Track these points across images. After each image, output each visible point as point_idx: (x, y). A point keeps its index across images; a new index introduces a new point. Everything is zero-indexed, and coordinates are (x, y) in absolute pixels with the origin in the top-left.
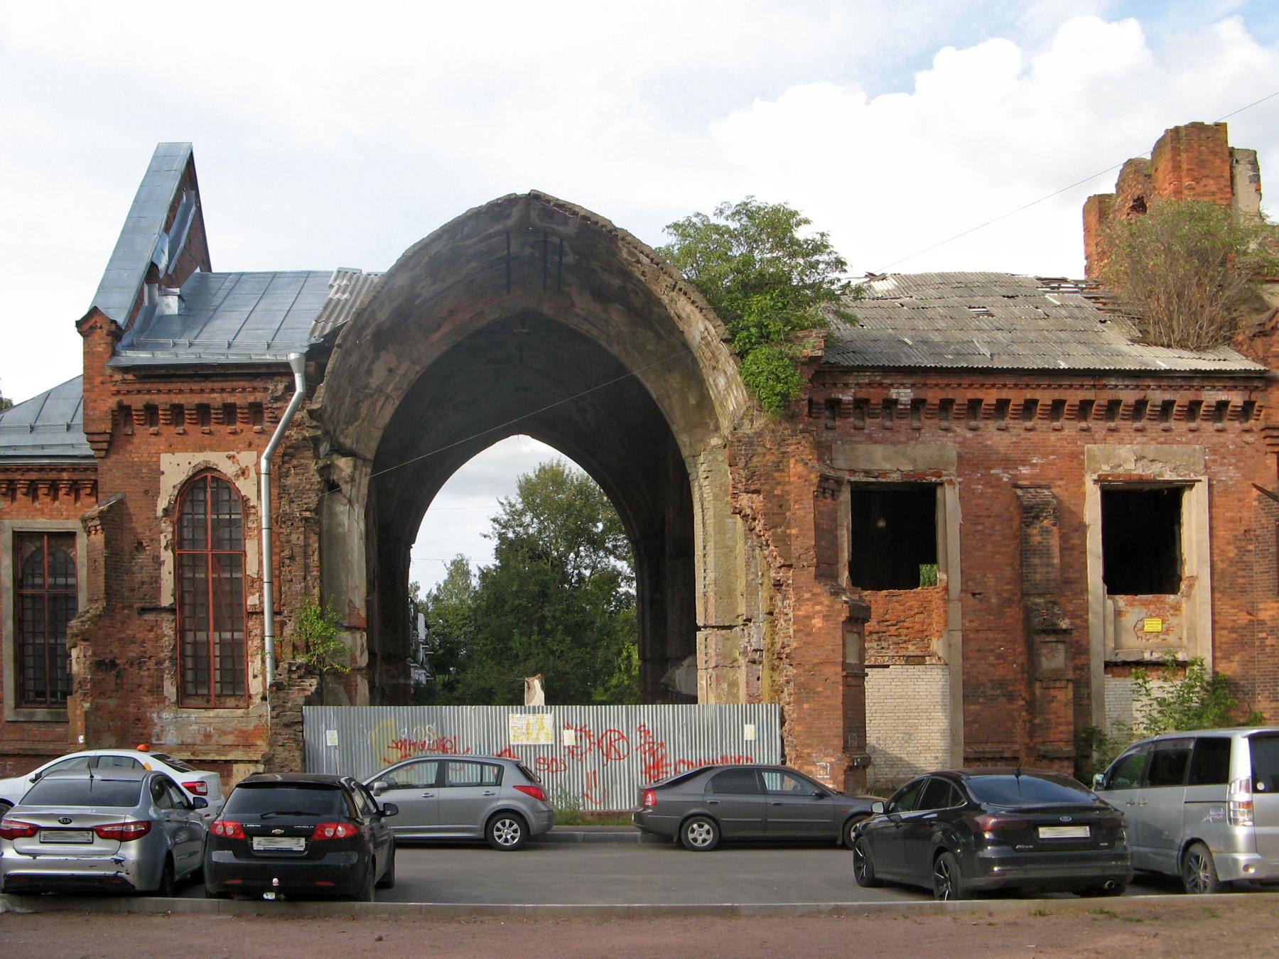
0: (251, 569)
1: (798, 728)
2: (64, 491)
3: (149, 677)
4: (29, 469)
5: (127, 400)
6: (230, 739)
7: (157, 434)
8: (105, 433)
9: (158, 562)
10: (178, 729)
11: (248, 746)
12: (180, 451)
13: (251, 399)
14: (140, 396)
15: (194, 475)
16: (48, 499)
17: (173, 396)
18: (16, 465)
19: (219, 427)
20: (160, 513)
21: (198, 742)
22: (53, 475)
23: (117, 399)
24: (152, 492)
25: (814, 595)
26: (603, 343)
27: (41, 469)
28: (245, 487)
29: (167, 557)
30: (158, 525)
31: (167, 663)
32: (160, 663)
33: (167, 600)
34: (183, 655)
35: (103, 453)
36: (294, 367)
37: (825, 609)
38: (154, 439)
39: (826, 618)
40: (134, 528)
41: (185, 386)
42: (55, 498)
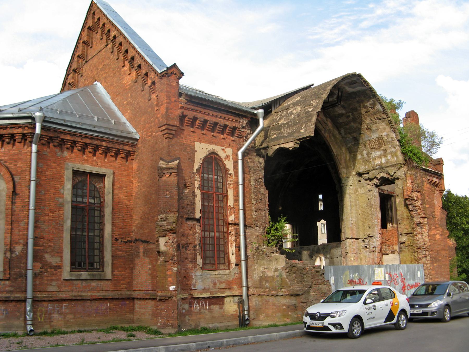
0: (231, 202)
1: (433, 272)
2: (100, 152)
3: (191, 254)
4: (86, 137)
5: (186, 113)
6: (223, 286)
7: (193, 132)
8: (176, 126)
9: (194, 195)
10: (203, 281)
11: (230, 288)
12: (203, 142)
13: (234, 125)
14: (192, 112)
15: (209, 155)
16: (91, 155)
17: (204, 115)
18: (80, 133)
19: (218, 134)
20: (195, 171)
21: (211, 287)
22: (97, 143)
23: (181, 111)
24: (192, 160)
25: (436, 227)
26: (323, 132)
27: (93, 138)
28: (229, 164)
29: (198, 192)
30: (194, 177)
31: (198, 247)
32: (195, 247)
33: (198, 215)
34: (204, 244)
35: (171, 136)
36: (37, 120)
37: (440, 232)
38: (192, 134)
39: (441, 235)
40: (184, 177)
41: (211, 112)
42: (94, 155)
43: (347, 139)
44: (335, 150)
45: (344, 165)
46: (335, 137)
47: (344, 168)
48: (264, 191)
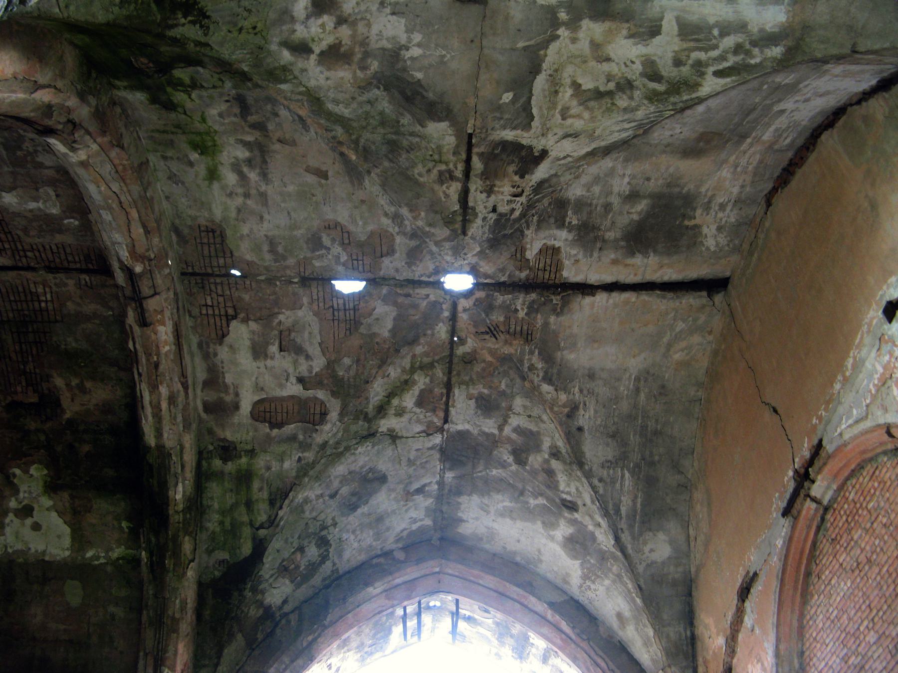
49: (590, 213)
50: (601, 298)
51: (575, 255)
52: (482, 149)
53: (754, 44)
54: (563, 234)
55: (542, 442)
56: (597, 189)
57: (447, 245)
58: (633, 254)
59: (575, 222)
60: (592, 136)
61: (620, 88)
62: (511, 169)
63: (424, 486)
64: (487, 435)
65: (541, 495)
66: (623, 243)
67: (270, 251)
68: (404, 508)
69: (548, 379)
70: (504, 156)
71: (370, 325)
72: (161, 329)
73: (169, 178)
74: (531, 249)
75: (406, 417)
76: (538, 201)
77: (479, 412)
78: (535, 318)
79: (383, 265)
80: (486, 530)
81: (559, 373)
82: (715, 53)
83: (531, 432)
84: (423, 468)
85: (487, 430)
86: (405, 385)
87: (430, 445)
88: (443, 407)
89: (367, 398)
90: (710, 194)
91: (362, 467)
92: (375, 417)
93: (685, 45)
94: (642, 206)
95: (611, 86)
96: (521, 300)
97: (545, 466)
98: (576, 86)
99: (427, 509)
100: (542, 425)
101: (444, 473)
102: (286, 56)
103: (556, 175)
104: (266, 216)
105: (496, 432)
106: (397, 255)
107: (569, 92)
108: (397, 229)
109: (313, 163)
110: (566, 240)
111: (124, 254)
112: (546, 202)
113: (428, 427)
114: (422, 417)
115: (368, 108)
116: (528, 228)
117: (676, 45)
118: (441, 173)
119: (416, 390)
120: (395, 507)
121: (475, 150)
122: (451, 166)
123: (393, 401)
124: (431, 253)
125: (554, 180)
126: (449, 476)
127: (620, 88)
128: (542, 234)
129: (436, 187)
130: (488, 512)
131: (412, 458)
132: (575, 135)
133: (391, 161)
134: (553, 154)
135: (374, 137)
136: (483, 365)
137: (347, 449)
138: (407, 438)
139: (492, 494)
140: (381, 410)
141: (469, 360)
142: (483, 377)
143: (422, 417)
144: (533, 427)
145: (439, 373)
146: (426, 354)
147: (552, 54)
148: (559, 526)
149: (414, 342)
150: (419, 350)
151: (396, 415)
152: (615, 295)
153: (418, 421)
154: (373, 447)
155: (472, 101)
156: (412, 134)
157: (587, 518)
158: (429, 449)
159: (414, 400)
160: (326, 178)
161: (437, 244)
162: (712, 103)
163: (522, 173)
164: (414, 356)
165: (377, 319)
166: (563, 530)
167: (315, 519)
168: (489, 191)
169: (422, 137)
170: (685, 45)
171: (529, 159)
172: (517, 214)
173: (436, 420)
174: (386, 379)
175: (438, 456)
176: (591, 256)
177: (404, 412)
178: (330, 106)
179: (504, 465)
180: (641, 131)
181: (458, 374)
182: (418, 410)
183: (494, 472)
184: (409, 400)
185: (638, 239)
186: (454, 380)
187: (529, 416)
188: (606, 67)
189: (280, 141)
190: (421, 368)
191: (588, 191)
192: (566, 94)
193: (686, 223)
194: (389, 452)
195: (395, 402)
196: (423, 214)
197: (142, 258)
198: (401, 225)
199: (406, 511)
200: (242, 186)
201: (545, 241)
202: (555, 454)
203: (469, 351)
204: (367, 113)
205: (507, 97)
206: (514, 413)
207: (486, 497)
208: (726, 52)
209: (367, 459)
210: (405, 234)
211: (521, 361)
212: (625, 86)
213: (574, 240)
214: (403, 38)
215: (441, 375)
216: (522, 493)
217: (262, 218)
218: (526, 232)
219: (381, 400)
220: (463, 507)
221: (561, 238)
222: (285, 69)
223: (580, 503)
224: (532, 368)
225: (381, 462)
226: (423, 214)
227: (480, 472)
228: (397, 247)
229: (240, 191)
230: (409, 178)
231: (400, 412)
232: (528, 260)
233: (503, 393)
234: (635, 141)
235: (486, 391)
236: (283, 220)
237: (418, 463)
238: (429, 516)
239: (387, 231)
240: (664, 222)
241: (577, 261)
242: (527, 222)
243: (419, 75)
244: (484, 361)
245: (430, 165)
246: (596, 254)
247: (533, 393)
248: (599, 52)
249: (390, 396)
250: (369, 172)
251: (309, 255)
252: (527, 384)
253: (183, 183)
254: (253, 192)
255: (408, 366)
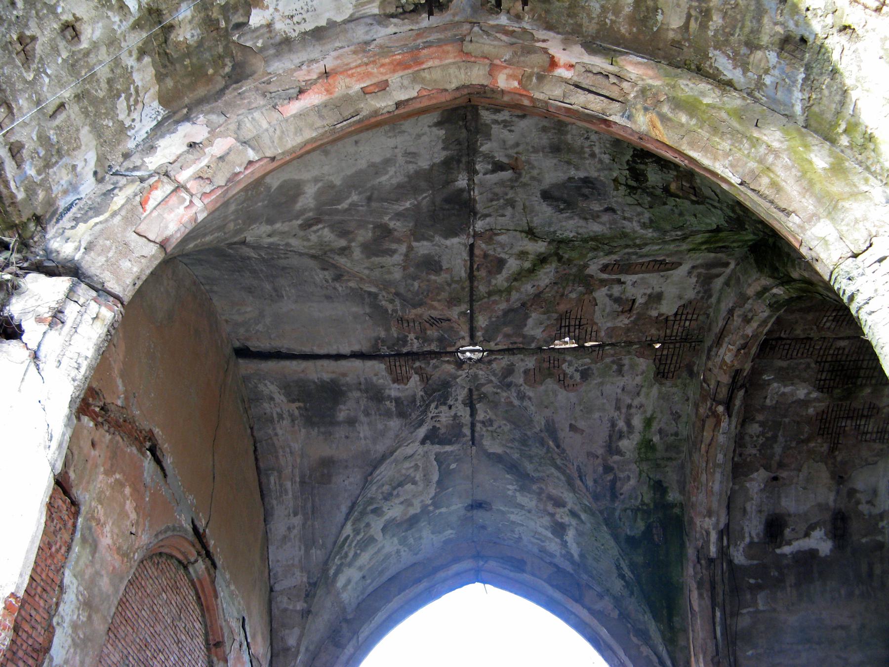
43: (768, 80)
44: (724, 162)
45: (808, 204)
46: (691, 107)
47: (813, 218)
48: (807, 548)
49: (378, 409)
50: (345, 350)
51: (379, 379)
52: (465, 439)
53: (342, 564)
54: (393, 393)
55: (362, 252)
56: (380, 426)
57: (482, 381)
58: (332, 380)
59: (388, 403)
60: (396, 461)
61: (391, 494)
62: (443, 431)
63: (493, 171)
64: (423, 238)
65: (346, 211)
66: (344, 388)
67: (624, 365)
68: (520, 149)
69: (374, 296)
70: (449, 437)
71: (548, 319)
72: (728, 358)
73: (680, 416)
74: (416, 382)
75: (517, 249)
76: (420, 416)
77: (436, 258)
78: (399, 334)
79: (534, 362)
80: (403, 128)
81: (363, 299)
82: (353, 545)
83: (377, 256)
84: (496, 194)
85: (425, 243)
86: (518, 277)
87: (488, 219)
88: (476, 259)
89: (557, 272)
90: (296, 428)
91: (571, 218)
92: (550, 255)
93: (368, 535)
94: (342, 416)
95: (395, 493)
96: (415, 347)
97: (351, 236)
98: (414, 483)
99: (488, 137)
100: (367, 265)
101: (468, 185)
102: (583, 516)
103: (412, 433)
104: (619, 391)
105: (414, 244)
106: (522, 370)
107: (417, 478)
108: (522, 388)
109: (578, 437)
110: (390, 389)
111: (724, 425)
112: (414, 416)
113: (491, 239)
114: (499, 250)
115: (539, 468)
116: (422, 396)
117: (372, 532)
118: (491, 425)
119: (505, 273)
120: (533, 157)
121: (469, 438)
122: (484, 429)
123: (530, 266)
124: (495, 375)
125: (412, 429)
126: (462, 182)
127: (391, 494)
128: (409, 393)
129: (494, 417)
130: (407, 154)
131: (509, 208)
132: (406, 458)
133: (526, 434)
134: (417, 443)
135: (537, 450)
136: (439, 298)
137: (585, 241)
138: (516, 230)
139: (406, 179)
140: (542, 260)
141: (453, 301)
142: (437, 288)
143: (499, 250)
144: (376, 260)
145: (482, 289)
146: (495, 302)
147: (432, 491)
148: (314, 198)
149: (506, 313)
150: (503, 306)
151: (527, 253)
152: (334, 352)
153: (503, 246)
154: (555, 232)
155: (475, 461)
156: (512, 448)
157: (286, 229)
158: (489, 215)
159: (507, 265)
160: (571, 425)
161: (491, 381)
162: (340, 516)
163: (434, 429)
164: (508, 300)
165: (541, 324)
166: (308, 200)
167: (639, 204)
168: (455, 417)
169: (504, 445)
170: (368, 535)
171: (432, 437)
172: (433, 406)
173: (483, 246)
174: (536, 283)
175: (479, 207)
176: (366, 379)
177: (519, 255)
178: (562, 478)
179: (398, 216)
180: (369, 478)
181: (463, 288)
182: (503, 256)
183: (408, 204)
184: (513, 265)
185: (333, 392)
186: (467, 284)
187: (382, 267)
188: (402, 499)
189: (598, 457)
190: (500, 292)
191: (386, 425)
192: (418, 476)
193: (301, 405)
194: (536, 221)
195: (527, 265)
196: (503, 400)
197: (715, 414)
198: (519, 392)
199: (517, 145)
200: (631, 415)
201: (407, 387)
202: (344, 251)
203: (455, 308)
204: (540, 465)
205: (453, 466)
206: (399, 265)
207: (412, 172)
208: (350, 549)
209: (564, 224)
210: (516, 385)
211: (403, 306)
212: (387, 497)
213: (384, 389)
214: (518, 494)
215: (480, 287)
216: (369, 199)
217: (623, 390)
218: (422, 393)
219: (543, 268)
220: (440, 145)
221: (394, 391)
222: (585, 512)
223: (302, 233)
224: (391, 301)
225: (548, 214)
226: (503, 400)
227: (424, 198)
228: (522, 375)
229: (633, 410)
230: (514, 423)
231: (522, 255)
232: (416, 373)
233: (414, 278)
234: (370, 470)
235: (433, 277)
236: (608, 389)
237: (502, 201)
238: (486, 125)
239: (530, 386)
240: (320, 404)
241: (376, 375)
242: (424, 401)
243: (508, 476)
244: (439, 301)
245: (498, 430)
246: (362, 380)
247: (386, 285)
248: (408, 503)
249: (532, 271)
250: (541, 431)
251: (593, 366)
252: (393, 290)
253: (672, 413)
254: (624, 410)
255: (514, 293)
